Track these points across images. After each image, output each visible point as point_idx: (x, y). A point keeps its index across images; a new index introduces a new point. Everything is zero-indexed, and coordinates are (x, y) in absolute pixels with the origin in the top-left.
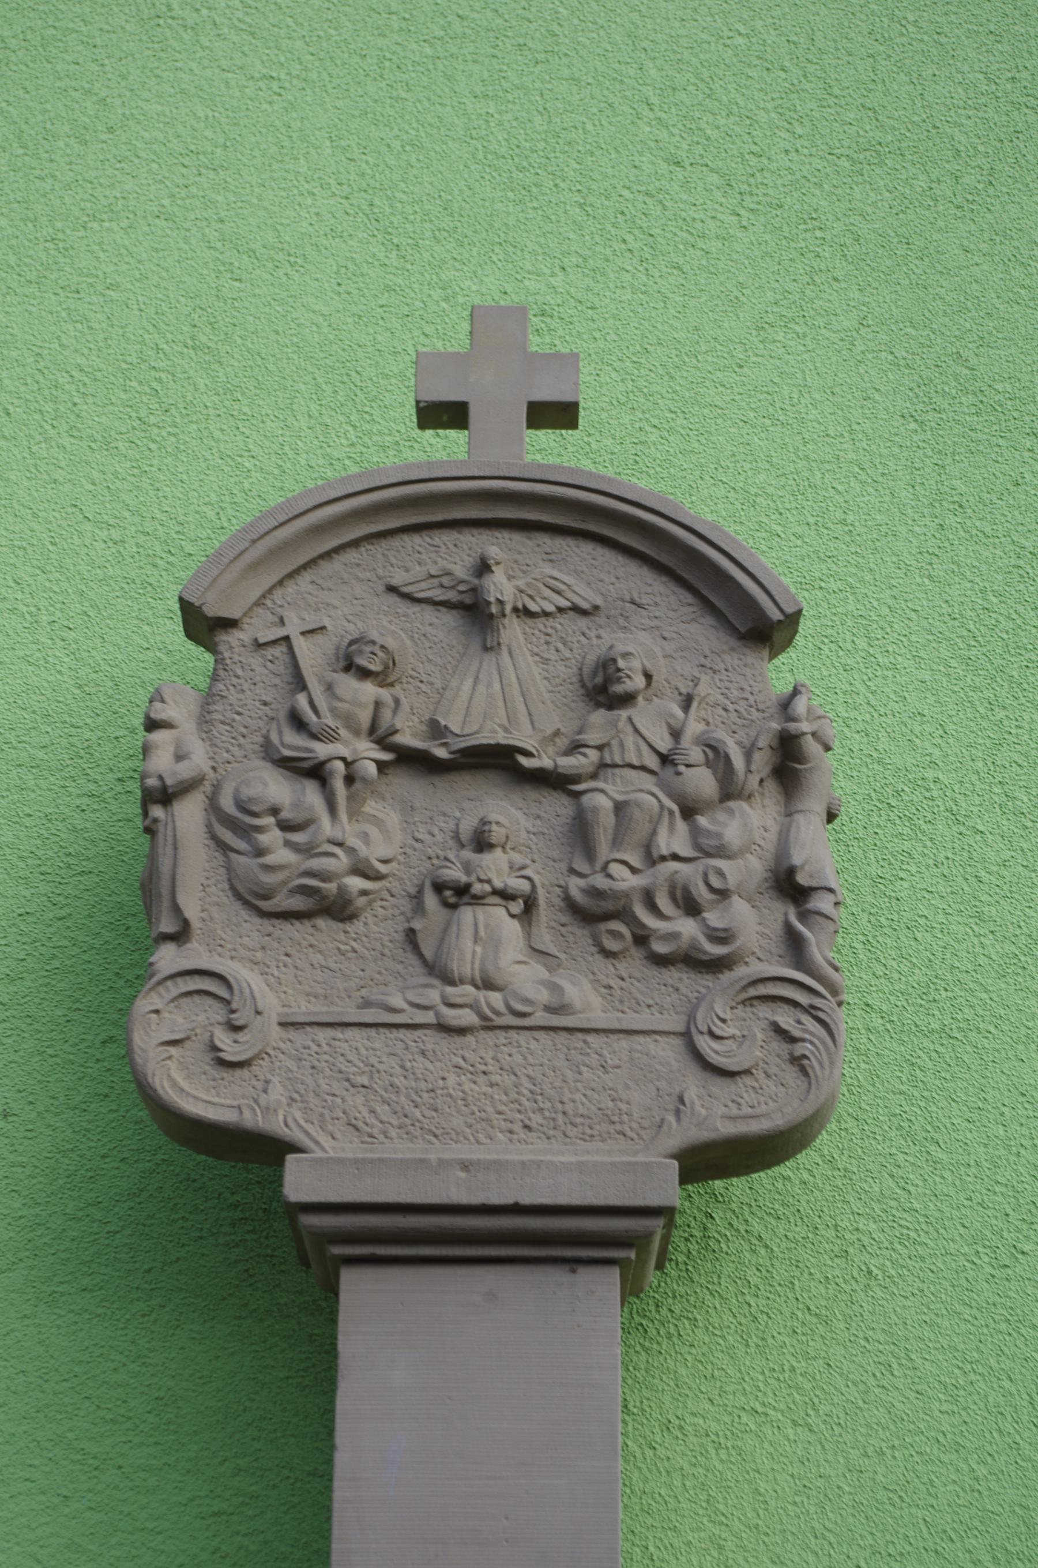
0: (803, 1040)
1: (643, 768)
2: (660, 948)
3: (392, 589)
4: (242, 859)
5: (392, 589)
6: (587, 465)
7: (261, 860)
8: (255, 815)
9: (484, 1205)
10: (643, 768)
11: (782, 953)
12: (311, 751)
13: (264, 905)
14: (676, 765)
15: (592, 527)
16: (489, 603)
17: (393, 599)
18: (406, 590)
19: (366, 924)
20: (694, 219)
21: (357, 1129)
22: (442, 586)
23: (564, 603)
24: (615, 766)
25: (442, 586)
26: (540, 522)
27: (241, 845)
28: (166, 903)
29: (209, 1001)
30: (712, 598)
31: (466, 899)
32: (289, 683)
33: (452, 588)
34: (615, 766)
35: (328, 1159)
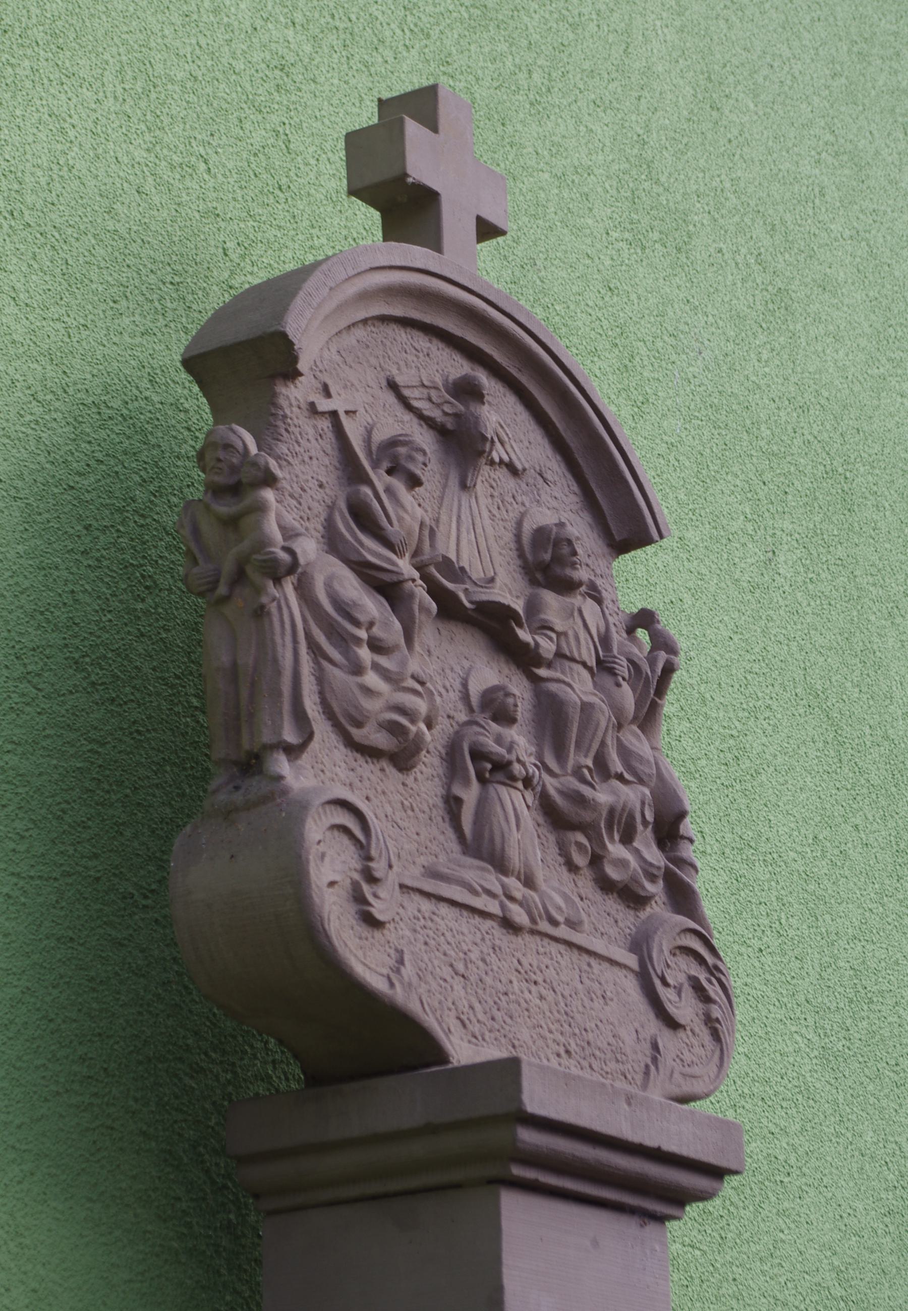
0: (714, 1002)
1: (584, 664)
2: (613, 873)
3: (393, 386)
4: (337, 672)
5: (393, 386)
6: (539, 313)
7: (359, 679)
8: (357, 623)
9: (641, 1145)
10: (584, 664)
11: (666, 901)
12: (394, 564)
13: (355, 732)
14: (615, 675)
15: (525, 380)
16: (484, 438)
17: (391, 398)
18: (406, 392)
19: (416, 779)
20: (377, 19)
21: (464, 1026)
22: (430, 399)
23: (506, 458)
24: (573, 660)
25: (430, 399)
26: (490, 357)
27: (334, 654)
28: (287, 707)
29: (346, 840)
30: (599, 495)
31: (500, 776)
32: (337, 469)
33: (438, 405)
34: (573, 660)
35: (548, 1067)
